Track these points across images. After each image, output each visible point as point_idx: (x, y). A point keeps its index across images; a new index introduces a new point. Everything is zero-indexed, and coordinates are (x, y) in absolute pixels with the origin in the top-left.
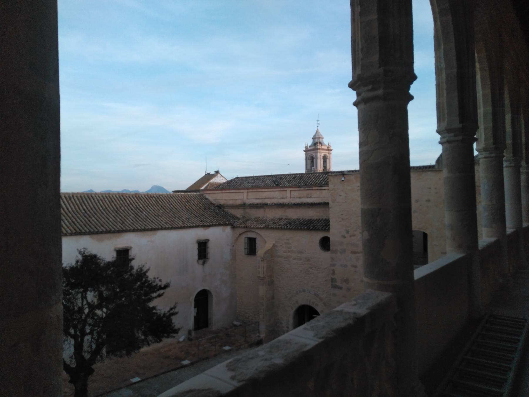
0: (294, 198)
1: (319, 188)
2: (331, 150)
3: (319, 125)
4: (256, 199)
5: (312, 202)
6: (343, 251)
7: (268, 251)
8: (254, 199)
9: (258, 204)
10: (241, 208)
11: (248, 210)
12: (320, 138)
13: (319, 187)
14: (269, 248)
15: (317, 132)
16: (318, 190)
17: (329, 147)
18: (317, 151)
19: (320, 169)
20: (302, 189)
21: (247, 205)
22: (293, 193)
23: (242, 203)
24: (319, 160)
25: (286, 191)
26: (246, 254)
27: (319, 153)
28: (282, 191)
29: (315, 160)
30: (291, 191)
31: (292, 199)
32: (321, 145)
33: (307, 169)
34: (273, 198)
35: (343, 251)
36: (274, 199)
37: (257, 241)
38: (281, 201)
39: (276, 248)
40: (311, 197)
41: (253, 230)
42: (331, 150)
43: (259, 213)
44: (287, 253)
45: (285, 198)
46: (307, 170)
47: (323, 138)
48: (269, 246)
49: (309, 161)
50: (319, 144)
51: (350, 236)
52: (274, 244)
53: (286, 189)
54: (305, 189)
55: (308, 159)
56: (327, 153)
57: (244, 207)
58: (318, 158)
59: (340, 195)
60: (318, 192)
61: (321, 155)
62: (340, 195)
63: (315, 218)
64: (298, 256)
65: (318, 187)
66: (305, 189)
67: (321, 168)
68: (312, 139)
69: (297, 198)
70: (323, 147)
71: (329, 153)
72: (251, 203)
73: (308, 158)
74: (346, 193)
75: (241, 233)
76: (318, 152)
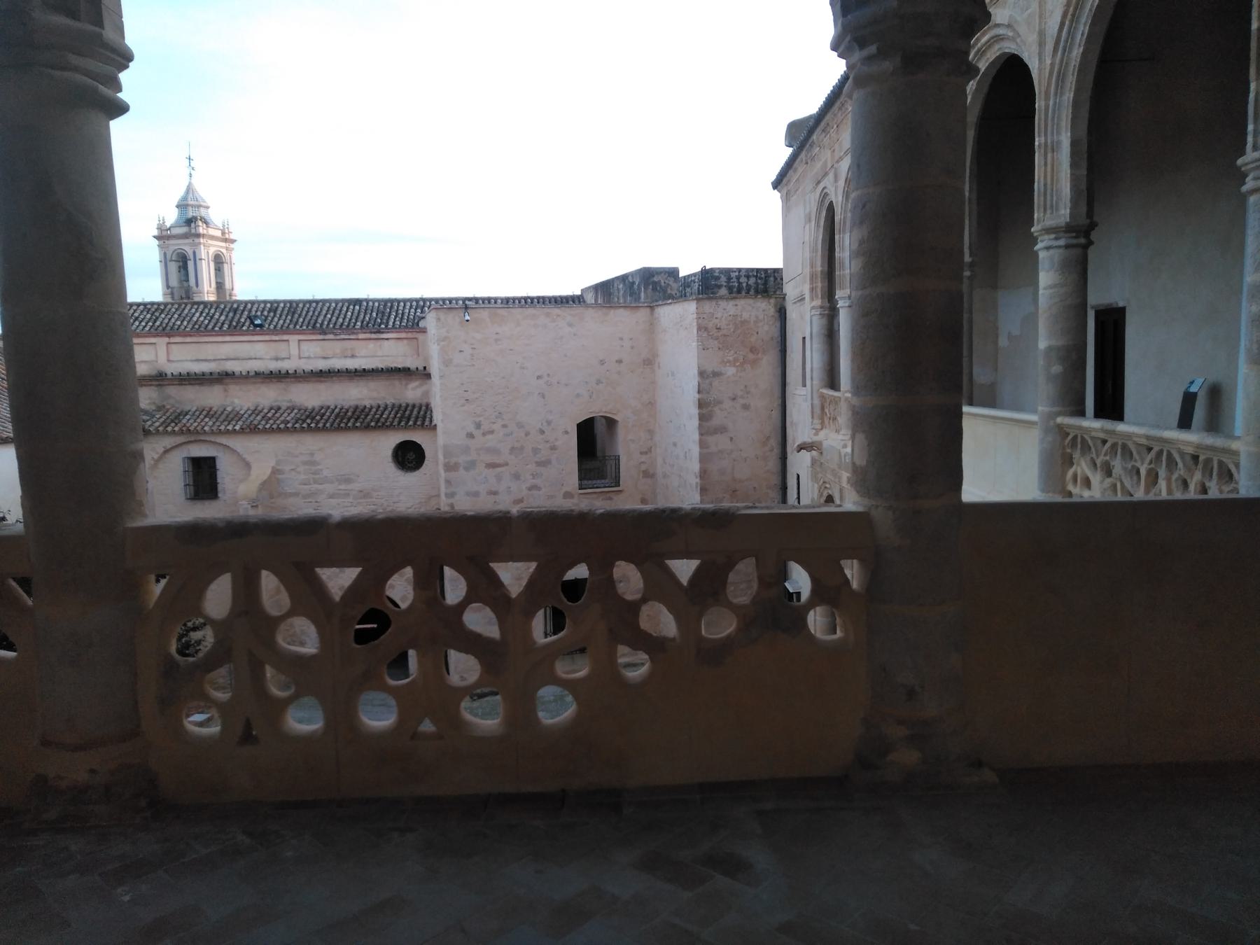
0: (309, 358)
1: (373, 336)
2: (233, 241)
3: (192, 172)
4: (197, 360)
5: (357, 366)
6: (471, 465)
7: (264, 483)
8: (192, 361)
9: (203, 374)
10: (151, 385)
11: (172, 391)
12: (199, 206)
13: (375, 333)
14: (265, 478)
15: (190, 189)
16: (370, 339)
17: (227, 231)
18: (197, 240)
19: (209, 289)
20: (331, 336)
21: (169, 376)
22: (305, 346)
23: (154, 373)
24: (204, 264)
25: (288, 341)
26: (188, 499)
27: (202, 247)
28: (276, 341)
29: (191, 265)
30: (299, 341)
31: (303, 360)
32: (208, 227)
33: (168, 287)
34: (251, 359)
35: (471, 465)
36: (254, 361)
37: (220, 465)
38: (274, 366)
39: (280, 476)
40: (353, 356)
41: (212, 438)
42: (233, 241)
43: (212, 397)
44: (310, 484)
45: (284, 359)
46: (170, 290)
47: (208, 207)
48: (261, 471)
49: (173, 267)
50: (200, 223)
51: (484, 434)
52: (273, 467)
53: (285, 337)
54: (338, 337)
55: (171, 260)
56: (221, 247)
57: (161, 383)
58: (201, 259)
59: (461, 351)
60: (371, 345)
61: (208, 252)
62: (461, 351)
63: (367, 403)
64: (340, 490)
65: (371, 333)
66: (338, 337)
67: (210, 286)
68: (177, 207)
69: (315, 358)
70: (212, 232)
71: (227, 249)
72: (184, 372)
73: (168, 257)
74: (473, 346)
75: (169, 447)
76: (200, 243)
